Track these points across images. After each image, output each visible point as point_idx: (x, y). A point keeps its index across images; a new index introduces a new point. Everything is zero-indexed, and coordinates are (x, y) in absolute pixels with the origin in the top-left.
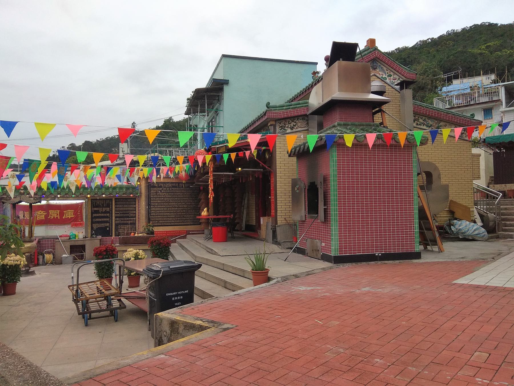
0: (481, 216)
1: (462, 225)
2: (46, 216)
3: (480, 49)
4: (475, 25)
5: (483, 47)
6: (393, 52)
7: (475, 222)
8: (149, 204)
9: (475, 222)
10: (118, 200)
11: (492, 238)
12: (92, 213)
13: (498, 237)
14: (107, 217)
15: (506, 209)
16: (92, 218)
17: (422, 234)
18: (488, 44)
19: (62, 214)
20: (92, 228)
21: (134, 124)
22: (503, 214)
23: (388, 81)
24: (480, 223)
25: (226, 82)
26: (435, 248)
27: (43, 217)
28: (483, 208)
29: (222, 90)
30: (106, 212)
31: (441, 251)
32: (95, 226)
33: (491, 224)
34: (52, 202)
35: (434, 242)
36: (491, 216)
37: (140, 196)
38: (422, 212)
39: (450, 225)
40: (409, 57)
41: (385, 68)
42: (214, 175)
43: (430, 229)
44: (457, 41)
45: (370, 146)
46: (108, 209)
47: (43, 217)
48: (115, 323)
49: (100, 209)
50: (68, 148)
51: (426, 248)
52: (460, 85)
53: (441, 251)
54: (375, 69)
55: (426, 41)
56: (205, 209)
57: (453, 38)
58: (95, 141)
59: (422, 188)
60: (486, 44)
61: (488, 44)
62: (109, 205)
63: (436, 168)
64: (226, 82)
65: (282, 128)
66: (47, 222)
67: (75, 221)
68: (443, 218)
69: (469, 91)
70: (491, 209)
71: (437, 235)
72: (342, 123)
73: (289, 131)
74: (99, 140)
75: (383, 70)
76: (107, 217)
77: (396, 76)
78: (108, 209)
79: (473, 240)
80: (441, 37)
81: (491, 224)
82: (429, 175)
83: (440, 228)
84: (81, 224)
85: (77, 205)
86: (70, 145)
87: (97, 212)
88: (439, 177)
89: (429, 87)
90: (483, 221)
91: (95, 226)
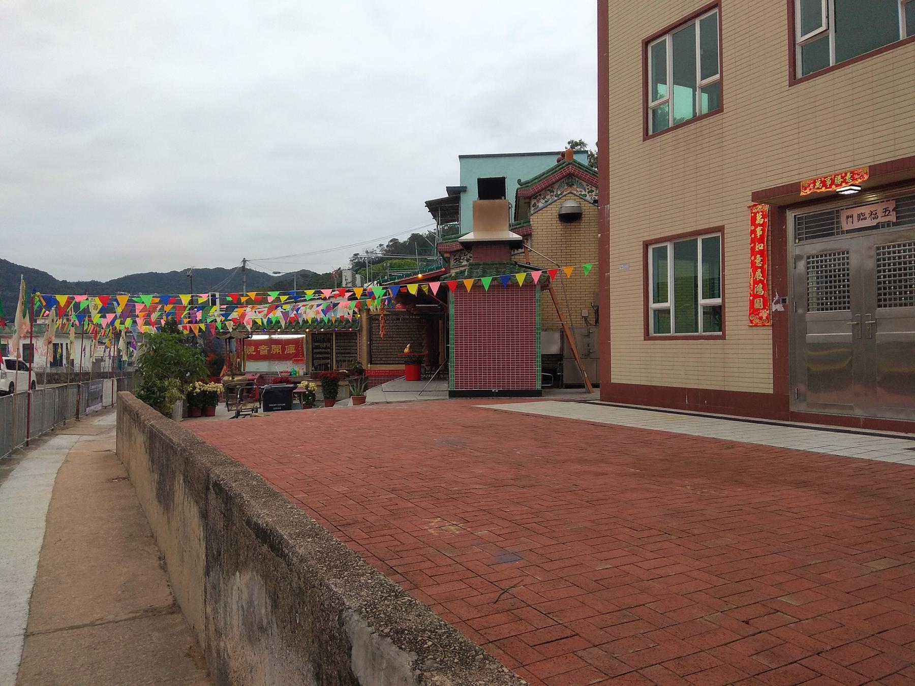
2: (269, 351)
8: (370, 339)
10: (338, 334)
12: (313, 349)
14: (327, 353)
16: (313, 354)
19: (283, 349)
20: (313, 364)
27: (266, 352)
30: (326, 348)
32: (316, 363)
34: (266, 337)
37: (360, 331)
41: (584, 184)
45: (469, 289)
46: (329, 345)
47: (266, 352)
48: (78, 423)
49: (321, 345)
62: (330, 340)
66: (258, 357)
67: (295, 357)
75: (581, 186)
76: (327, 353)
78: (329, 345)
80: (64, 282)
84: (302, 360)
85: (298, 339)
87: (318, 347)
91: (316, 363)
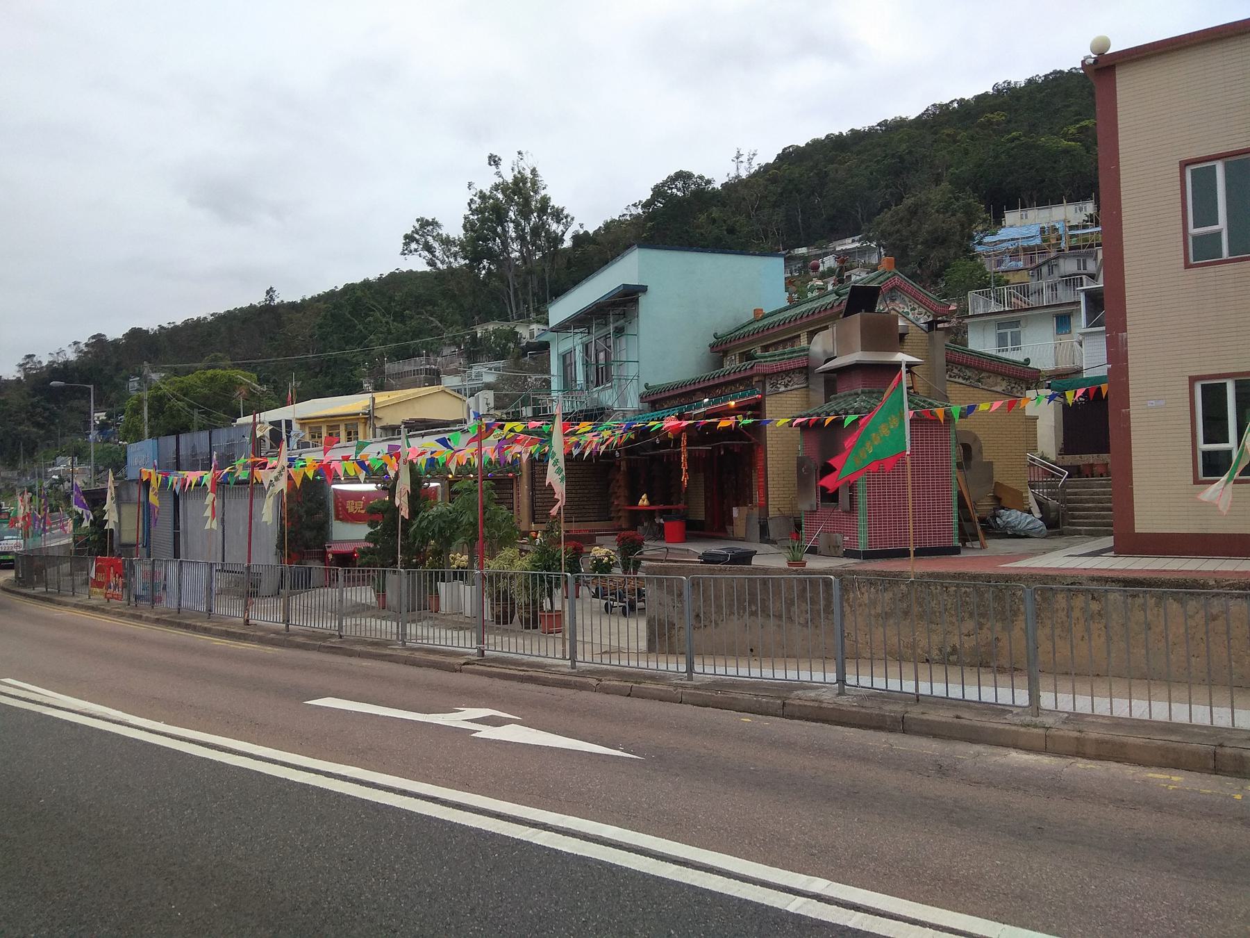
0: (1039, 504)
1: (1013, 517)
3: (1065, 136)
4: (1055, 72)
5: (1072, 130)
6: (871, 129)
7: (1030, 512)
9: (1030, 512)
11: (1053, 534)
13: (1061, 534)
15: (1075, 494)
17: (961, 527)
18: (1083, 123)
21: (270, 292)
22: (1069, 501)
23: (910, 316)
24: (1038, 515)
25: (643, 289)
26: (977, 544)
28: (1042, 492)
29: (636, 301)
31: (983, 547)
33: (1053, 515)
35: (975, 537)
36: (1053, 503)
38: (961, 497)
39: (994, 517)
40: (910, 152)
42: (689, 452)
43: (970, 520)
44: (1016, 110)
50: (87, 345)
51: (964, 545)
52: (1022, 225)
53: (983, 547)
54: (893, 301)
55: (947, 105)
56: (644, 496)
57: (1006, 101)
58: (156, 328)
59: (959, 466)
60: (1077, 121)
61: (1083, 123)
63: (976, 439)
64: (643, 289)
65: (774, 385)
68: (986, 506)
69: (1038, 241)
70: (1054, 494)
71: (979, 528)
72: (866, 389)
73: (782, 389)
74: (165, 325)
75: (904, 302)
77: (921, 310)
79: (1027, 537)
81: (1053, 515)
82: (967, 448)
83: (982, 520)
86: (93, 337)
88: (980, 451)
89: (957, 238)
90: (1041, 512)
